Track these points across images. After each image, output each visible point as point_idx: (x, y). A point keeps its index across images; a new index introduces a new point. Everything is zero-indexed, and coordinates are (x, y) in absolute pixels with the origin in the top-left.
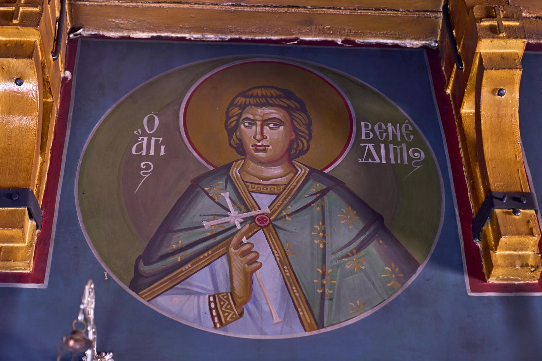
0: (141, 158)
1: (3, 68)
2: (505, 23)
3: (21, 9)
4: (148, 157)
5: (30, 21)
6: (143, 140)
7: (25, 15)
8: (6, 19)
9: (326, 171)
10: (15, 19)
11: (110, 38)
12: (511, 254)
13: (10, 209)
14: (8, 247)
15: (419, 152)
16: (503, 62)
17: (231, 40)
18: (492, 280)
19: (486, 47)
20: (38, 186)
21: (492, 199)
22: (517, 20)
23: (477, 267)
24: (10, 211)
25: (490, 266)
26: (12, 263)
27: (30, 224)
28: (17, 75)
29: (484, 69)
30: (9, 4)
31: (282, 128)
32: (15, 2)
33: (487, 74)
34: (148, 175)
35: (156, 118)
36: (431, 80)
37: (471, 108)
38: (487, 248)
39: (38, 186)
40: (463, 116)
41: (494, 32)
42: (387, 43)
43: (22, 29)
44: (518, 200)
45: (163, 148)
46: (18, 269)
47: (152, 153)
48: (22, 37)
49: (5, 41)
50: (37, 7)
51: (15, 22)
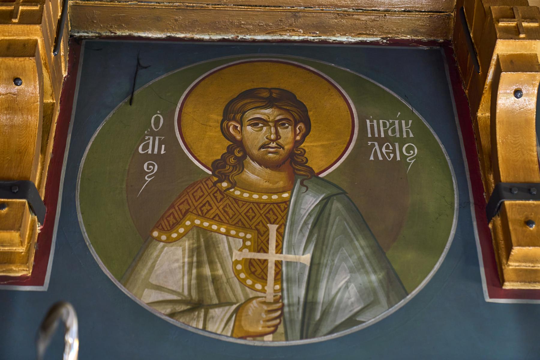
2: (525, 24)
3: (21, 8)
6: (149, 139)
8: (5, 18)
12: (521, 258)
15: (154, 166)
17: (220, 40)
18: (508, 286)
19: (503, 48)
20: (38, 177)
21: (503, 191)
23: (497, 278)
27: (30, 217)
29: (501, 72)
32: (14, 1)
33: (505, 76)
39: (38, 177)
41: (513, 34)
44: (528, 190)
45: (163, 146)
50: (37, 5)
51: (14, 21)
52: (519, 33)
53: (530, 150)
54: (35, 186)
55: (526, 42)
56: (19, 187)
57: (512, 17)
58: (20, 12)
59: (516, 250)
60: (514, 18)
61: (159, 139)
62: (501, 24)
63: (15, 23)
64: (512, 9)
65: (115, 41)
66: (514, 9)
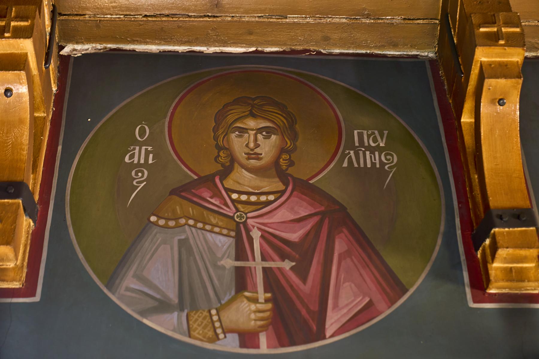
0: (132, 166)
1: (489, 89)
2: (503, 30)
4: (139, 165)
5: (19, 33)
6: (134, 149)
7: (16, 28)
9: (311, 182)
10: (7, 33)
11: (126, 50)
13: (519, 229)
14: (517, 267)
15: (392, 156)
16: (502, 71)
19: (483, 56)
20: (34, 182)
22: (517, 27)
23: (480, 281)
24: (521, 232)
25: (488, 281)
26: (526, 284)
28: (501, 95)
30: (489, 25)
31: (273, 137)
33: (489, 83)
34: (142, 185)
35: (146, 127)
36: (429, 92)
37: (471, 118)
38: (485, 263)
40: (462, 124)
41: (493, 39)
42: (134, 51)
43: (509, 50)
44: (520, 217)
45: (151, 156)
46: (528, 290)
47: (142, 161)
48: (504, 58)
49: (488, 61)
50: (27, 21)
51: (6, 35)
52: (4, 32)
53: (21, 149)
54: (29, 188)
55: (12, 41)
56: (13, 188)
57: (493, 23)
58: (11, 27)
59: (502, 253)
60: (495, 23)
61: (146, 149)
62: (482, 30)
63: (502, 45)
64: (494, 15)
65: (365, 59)
66: (496, 15)
